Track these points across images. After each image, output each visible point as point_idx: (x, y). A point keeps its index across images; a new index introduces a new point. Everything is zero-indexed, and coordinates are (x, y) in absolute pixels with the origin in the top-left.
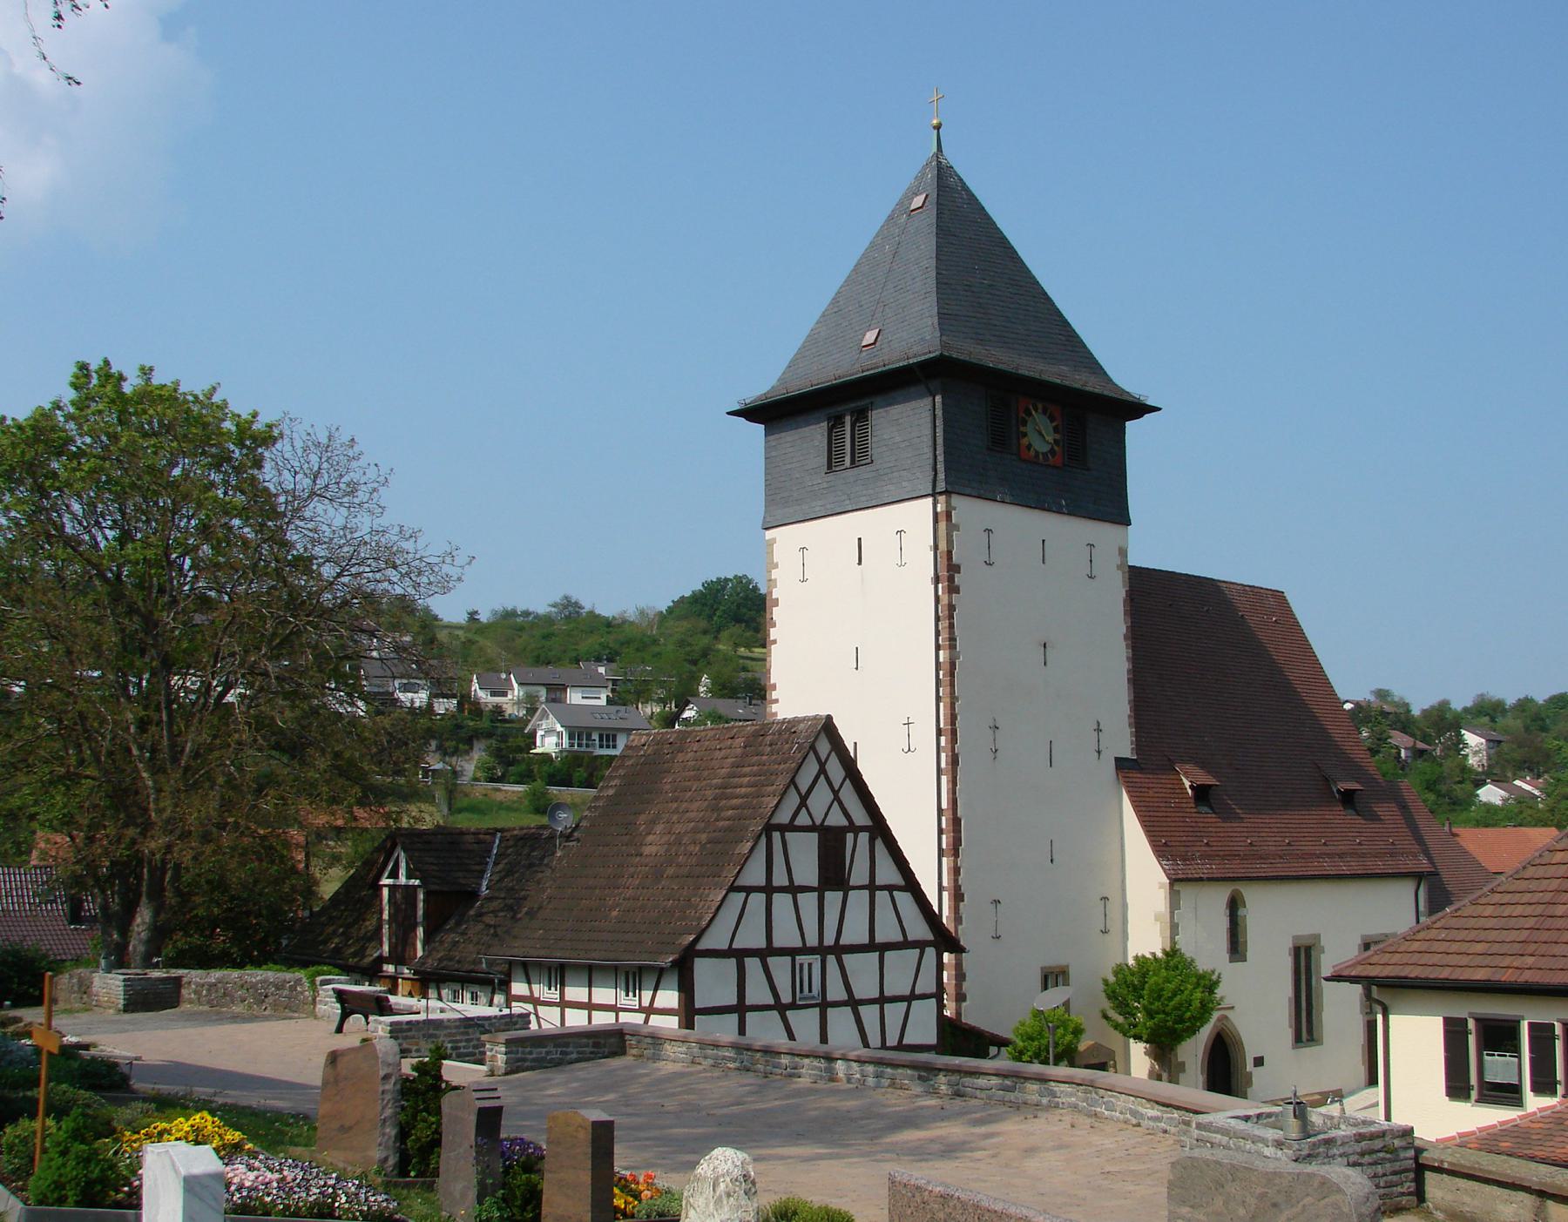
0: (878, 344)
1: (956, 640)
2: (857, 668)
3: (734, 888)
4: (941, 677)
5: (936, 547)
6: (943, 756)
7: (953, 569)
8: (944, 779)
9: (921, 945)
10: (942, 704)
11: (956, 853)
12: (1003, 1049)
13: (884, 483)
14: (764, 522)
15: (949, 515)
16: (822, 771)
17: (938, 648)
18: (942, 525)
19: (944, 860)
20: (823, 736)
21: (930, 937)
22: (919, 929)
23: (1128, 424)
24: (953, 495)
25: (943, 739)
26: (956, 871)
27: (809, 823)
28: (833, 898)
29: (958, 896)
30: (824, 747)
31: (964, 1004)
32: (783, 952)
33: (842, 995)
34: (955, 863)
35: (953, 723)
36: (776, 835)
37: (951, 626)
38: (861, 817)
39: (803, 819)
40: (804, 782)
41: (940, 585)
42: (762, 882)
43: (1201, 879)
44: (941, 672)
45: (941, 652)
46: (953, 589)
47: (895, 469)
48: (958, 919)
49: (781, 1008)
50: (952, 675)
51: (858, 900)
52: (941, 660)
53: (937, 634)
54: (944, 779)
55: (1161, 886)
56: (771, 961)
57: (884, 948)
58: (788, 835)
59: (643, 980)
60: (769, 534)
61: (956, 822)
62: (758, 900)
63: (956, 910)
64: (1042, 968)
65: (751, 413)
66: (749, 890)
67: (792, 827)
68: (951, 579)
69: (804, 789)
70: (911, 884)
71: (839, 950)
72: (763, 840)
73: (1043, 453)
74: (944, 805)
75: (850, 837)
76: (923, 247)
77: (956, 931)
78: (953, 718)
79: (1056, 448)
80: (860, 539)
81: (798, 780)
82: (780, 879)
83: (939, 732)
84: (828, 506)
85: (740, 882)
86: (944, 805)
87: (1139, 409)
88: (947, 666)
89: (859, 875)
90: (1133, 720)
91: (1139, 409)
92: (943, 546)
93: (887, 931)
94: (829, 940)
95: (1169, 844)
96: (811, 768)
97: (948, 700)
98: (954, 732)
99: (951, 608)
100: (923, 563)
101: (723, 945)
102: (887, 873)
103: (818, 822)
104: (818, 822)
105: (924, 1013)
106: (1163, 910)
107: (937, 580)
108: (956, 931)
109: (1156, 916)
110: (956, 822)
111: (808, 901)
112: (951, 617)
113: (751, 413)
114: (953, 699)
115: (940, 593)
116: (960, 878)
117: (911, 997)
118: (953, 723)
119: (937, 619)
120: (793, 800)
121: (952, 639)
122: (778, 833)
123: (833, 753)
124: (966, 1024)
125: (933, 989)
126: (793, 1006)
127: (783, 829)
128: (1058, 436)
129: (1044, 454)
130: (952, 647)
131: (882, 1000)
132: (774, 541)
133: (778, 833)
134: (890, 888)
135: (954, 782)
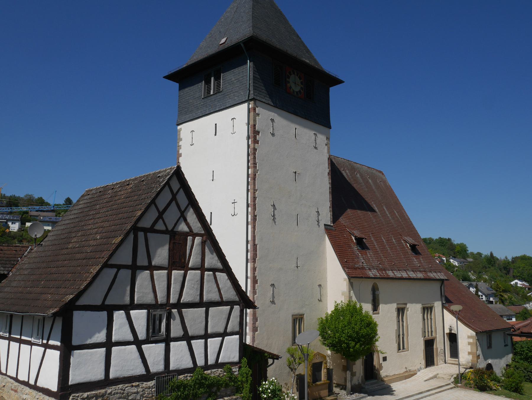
0: (226, 43)
1: (256, 164)
2: (213, 180)
3: (106, 265)
4: (249, 181)
5: (248, 124)
6: (250, 216)
7: (256, 133)
8: (250, 227)
9: (231, 304)
10: (249, 193)
11: (254, 260)
12: (275, 361)
13: (226, 99)
14: (178, 122)
15: (254, 110)
16: (174, 198)
17: (248, 168)
18: (252, 114)
19: (249, 264)
20: (175, 178)
21: (237, 299)
22: (229, 294)
23: (331, 88)
24: (257, 101)
25: (250, 209)
26: (254, 269)
27: (164, 228)
28: (176, 274)
29: (255, 281)
30: (175, 185)
31: (256, 333)
32: (140, 307)
33: (180, 333)
34: (254, 265)
35: (254, 201)
36: (141, 235)
37: (255, 158)
38: (196, 226)
39: (160, 226)
40: (162, 203)
41: (250, 140)
42: (130, 263)
43: (362, 277)
44: (250, 179)
45: (250, 170)
46: (256, 142)
47: (232, 92)
48: (254, 292)
49: (138, 343)
50: (254, 179)
51: (193, 275)
52: (250, 173)
53: (248, 161)
54: (250, 227)
55: (345, 280)
56: (133, 313)
57: (209, 305)
58: (149, 234)
59: (56, 320)
60: (179, 127)
61: (255, 246)
62: (125, 274)
63: (254, 288)
64: (292, 316)
65: (171, 77)
66: (119, 267)
67: (152, 230)
68: (255, 137)
69: (161, 208)
70: (227, 269)
71: (180, 306)
72: (131, 236)
73: (296, 92)
74: (250, 239)
75: (190, 238)
76: (247, 6)
77: (254, 298)
78: (254, 198)
79: (301, 91)
80: (216, 124)
81: (157, 201)
82: (142, 261)
83: (248, 206)
84: (203, 112)
85: (112, 262)
86: (250, 239)
87: (337, 82)
88: (253, 176)
89: (194, 260)
90: (331, 209)
91: (337, 82)
92: (252, 123)
93: (210, 294)
94: (173, 300)
95: (348, 262)
96: (166, 196)
97: (252, 191)
98: (255, 205)
99: (255, 150)
100: (242, 130)
101: (98, 302)
102: (211, 260)
103: (170, 228)
104: (170, 228)
105: (232, 342)
106: (346, 291)
107: (248, 138)
108: (254, 298)
109: (342, 293)
110: (255, 246)
111: (160, 275)
112: (254, 154)
113: (171, 77)
114: (255, 190)
115: (250, 143)
116: (256, 273)
117: (224, 334)
118: (254, 201)
119: (248, 155)
120: (153, 214)
121: (255, 164)
122: (142, 233)
123: (181, 190)
124: (256, 348)
125: (237, 329)
126: (147, 341)
127: (146, 231)
128: (302, 86)
129: (297, 92)
130: (255, 167)
131: (206, 336)
132: (181, 129)
133: (142, 233)
134: (214, 270)
135: (254, 228)
